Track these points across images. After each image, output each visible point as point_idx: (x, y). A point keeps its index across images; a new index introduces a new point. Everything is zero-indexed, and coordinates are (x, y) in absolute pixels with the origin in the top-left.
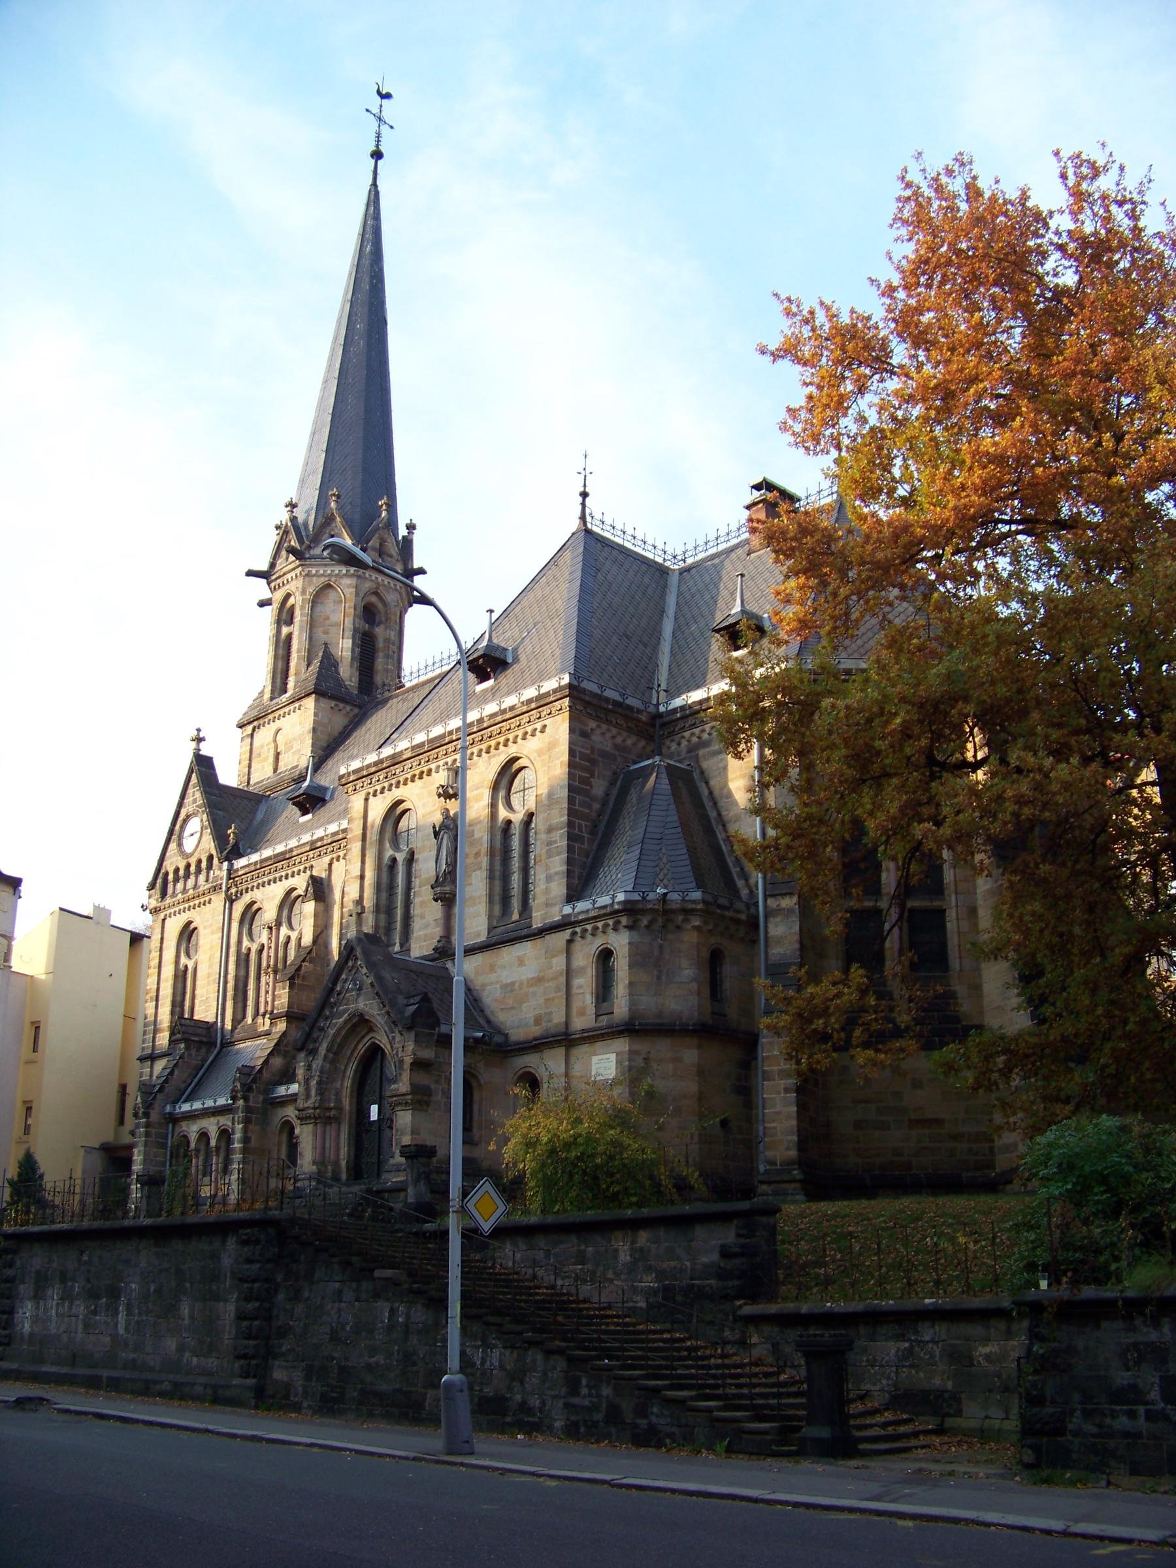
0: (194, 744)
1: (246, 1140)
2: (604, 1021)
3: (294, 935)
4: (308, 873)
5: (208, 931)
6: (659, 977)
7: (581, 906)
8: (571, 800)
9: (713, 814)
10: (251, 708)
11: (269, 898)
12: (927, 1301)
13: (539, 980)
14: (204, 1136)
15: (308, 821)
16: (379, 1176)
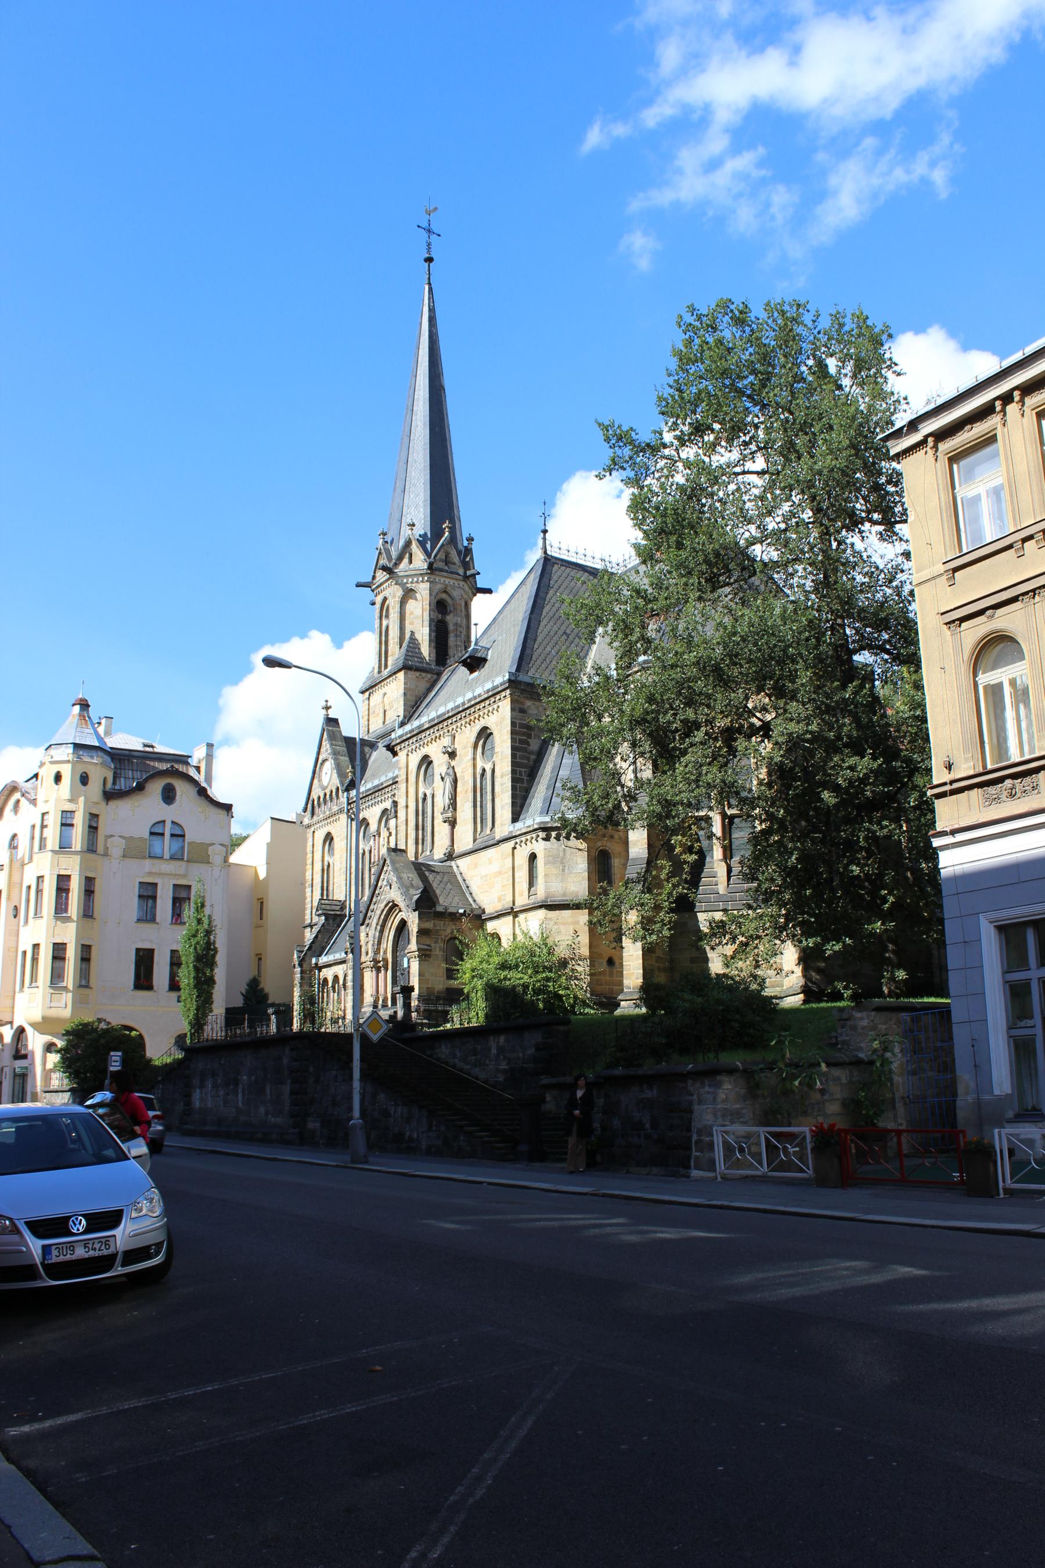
0: (324, 712)
2: (533, 899)
6: (563, 870)
7: (519, 825)
8: (513, 756)
10: (368, 678)
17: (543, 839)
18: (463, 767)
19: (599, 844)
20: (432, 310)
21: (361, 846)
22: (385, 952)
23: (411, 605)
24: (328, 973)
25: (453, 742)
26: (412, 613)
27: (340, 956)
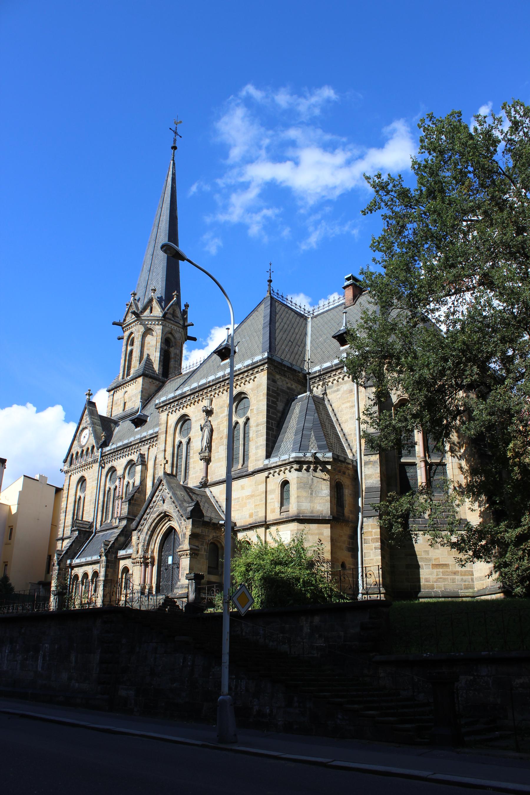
0: (87, 397)
1: (106, 576)
2: (284, 515)
3: (131, 482)
4: (138, 453)
5: (91, 480)
6: (311, 494)
9: (334, 419)
11: (120, 464)
12: (483, 653)
13: (252, 496)
14: (86, 575)
15: (139, 430)
16: (172, 590)
17: (296, 470)
18: (220, 423)
19: (337, 477)
20: (174, 174)
21: (108, 485)
22: (153, 552)
23: (149, 338)
24: (79, 572)
25: (211, 404)
26: (149, 343)
27: (95, 558)
